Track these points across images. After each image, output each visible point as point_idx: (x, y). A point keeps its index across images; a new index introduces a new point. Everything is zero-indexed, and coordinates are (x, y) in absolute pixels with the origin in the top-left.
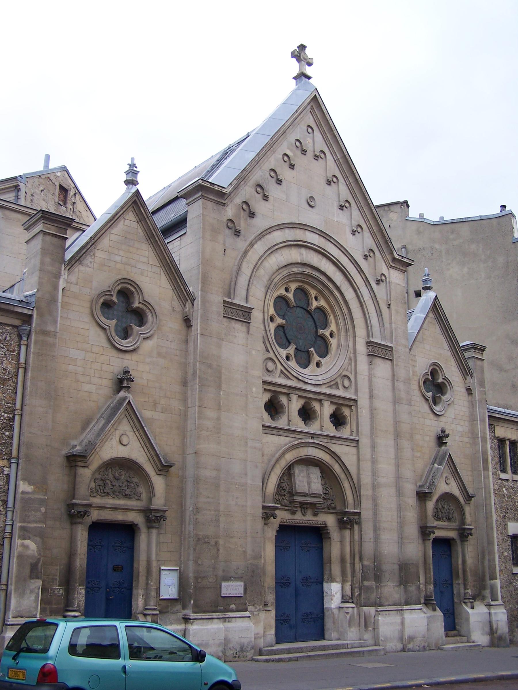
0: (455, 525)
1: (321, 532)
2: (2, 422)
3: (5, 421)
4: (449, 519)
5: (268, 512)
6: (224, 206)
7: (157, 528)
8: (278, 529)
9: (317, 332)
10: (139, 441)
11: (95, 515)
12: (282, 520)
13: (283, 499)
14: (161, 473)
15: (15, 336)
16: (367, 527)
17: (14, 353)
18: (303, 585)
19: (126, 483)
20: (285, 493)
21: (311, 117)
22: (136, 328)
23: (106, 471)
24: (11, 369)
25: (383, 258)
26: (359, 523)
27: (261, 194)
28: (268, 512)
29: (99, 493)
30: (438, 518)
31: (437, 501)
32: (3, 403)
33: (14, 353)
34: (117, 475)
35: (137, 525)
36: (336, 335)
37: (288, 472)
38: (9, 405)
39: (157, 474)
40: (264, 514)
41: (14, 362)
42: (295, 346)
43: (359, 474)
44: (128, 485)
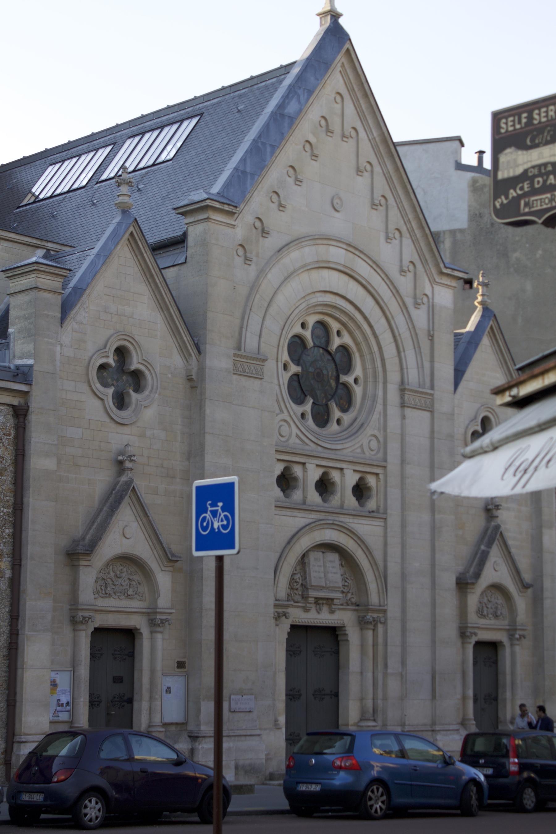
0: (504, 623)
1: (337, 633)
2: (2, 519)
3: (5, 517)
4: (496, 616)
5: (280, 610)
6: (234, 228)
7: (162, 632)
8: (289, 630)
9: (337, 378)
10: (143, 533)
11: (101, 621)
12: (294, 620)
13: (296, 594)
14: (167, 569)
15: (10, 416)
16: (394, 627)
17: (10, 437)
18: (315, 698)
19: (127, 581)
20: (297, 587)
21: (341, 78)
22: (134, 396)
23: (108, 568)
24: (8, 455)
25: (426, 271)
26: (385, 623)
27: (277, 203)
28: (280, 610)
29: (100, 594)
30: (482, 615)
31: (482, 593)
32: (2, 496)
33: (10, 437)
34: (118, 573)
35: (139, 629)
36: (361, 381)
37: (303, 560)
38: (7, 498)
39: (162, 570)
40: (276, 614)
41: (11, 448)
42: (312, 401)
43: (385, 561)
44: (130, 584)
